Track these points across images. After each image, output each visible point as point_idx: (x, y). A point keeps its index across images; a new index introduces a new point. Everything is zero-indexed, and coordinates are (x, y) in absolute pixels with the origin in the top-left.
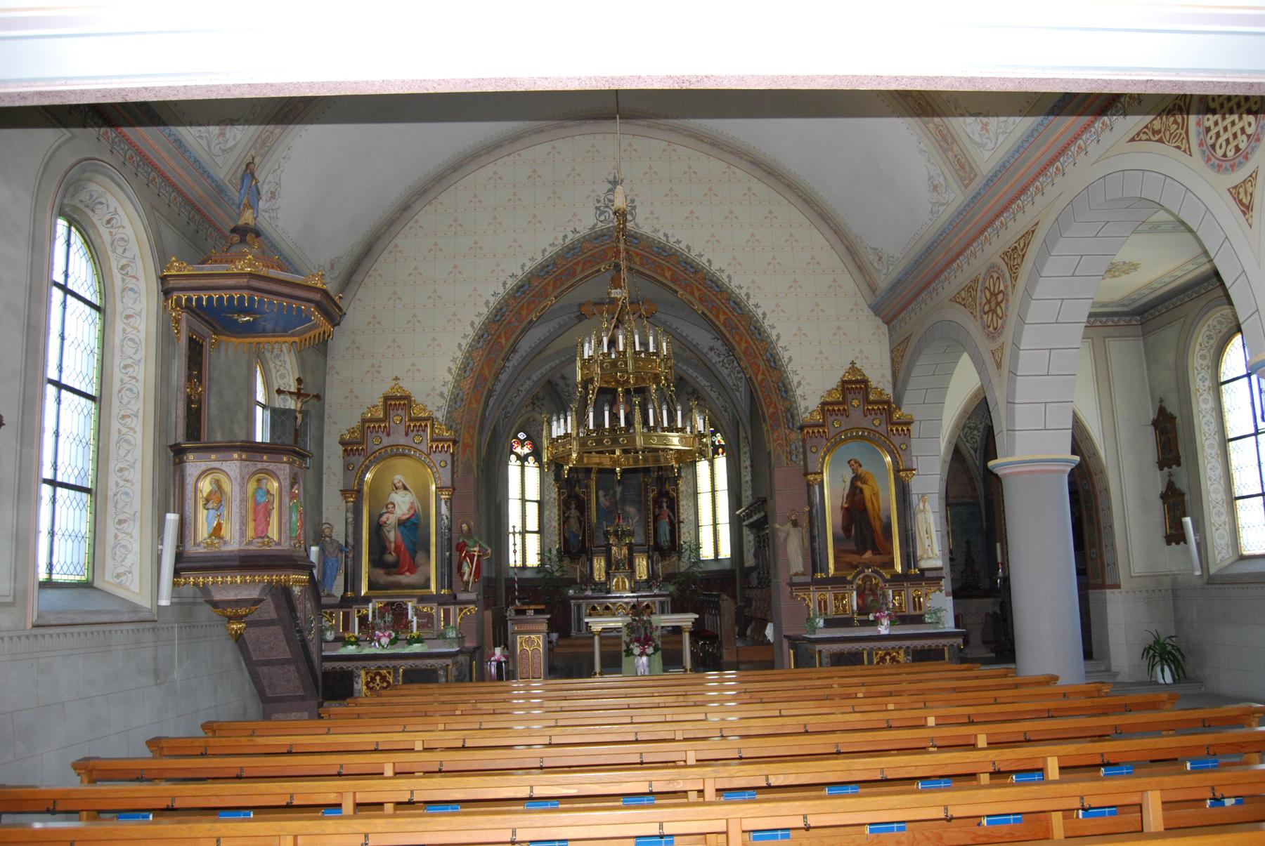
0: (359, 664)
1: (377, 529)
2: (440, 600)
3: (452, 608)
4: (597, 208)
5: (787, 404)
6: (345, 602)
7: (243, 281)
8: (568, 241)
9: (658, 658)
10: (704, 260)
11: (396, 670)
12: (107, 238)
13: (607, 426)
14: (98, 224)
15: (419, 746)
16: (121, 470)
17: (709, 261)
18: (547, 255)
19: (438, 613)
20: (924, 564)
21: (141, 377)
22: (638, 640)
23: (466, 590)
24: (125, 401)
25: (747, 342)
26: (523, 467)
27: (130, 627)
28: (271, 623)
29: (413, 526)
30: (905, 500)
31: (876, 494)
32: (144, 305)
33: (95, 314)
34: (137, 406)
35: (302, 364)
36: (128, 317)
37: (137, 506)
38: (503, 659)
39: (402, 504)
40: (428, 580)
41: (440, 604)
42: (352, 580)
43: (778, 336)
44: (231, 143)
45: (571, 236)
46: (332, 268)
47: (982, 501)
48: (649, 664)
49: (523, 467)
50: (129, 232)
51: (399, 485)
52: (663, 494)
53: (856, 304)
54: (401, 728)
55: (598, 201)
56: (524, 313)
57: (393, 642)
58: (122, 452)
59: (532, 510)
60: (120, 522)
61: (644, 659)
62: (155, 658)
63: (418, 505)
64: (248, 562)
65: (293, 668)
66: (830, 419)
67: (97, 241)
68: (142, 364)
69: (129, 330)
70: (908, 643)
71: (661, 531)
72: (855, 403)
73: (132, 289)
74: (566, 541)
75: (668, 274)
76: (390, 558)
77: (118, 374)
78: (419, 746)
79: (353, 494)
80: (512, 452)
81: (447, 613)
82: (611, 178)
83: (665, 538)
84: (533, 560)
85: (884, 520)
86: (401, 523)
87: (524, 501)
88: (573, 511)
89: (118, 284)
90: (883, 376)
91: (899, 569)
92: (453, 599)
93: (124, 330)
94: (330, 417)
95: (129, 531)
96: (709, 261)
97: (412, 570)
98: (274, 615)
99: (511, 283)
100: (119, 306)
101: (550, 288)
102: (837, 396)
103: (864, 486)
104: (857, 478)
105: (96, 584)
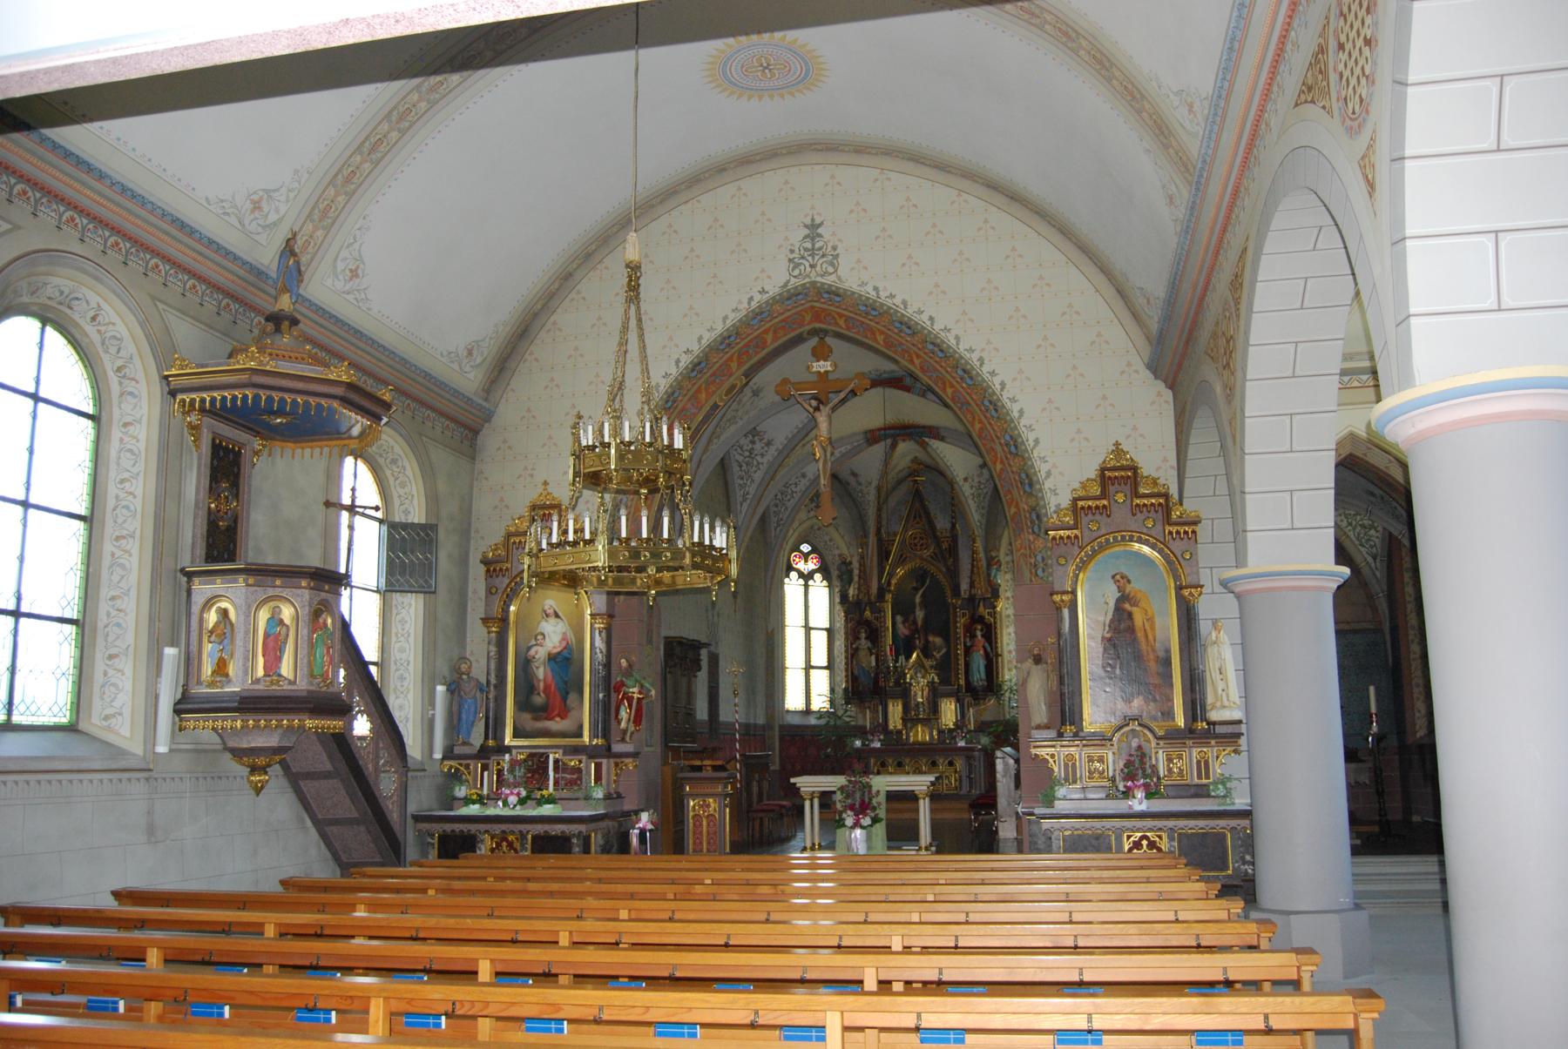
0: (482, 827)
1: (525, 664)
2: (591, 752)
3: (604, 761)
4: (790, 260)
5: (1032, 502)
6: (483, 753)
7: (244, 377)
8: (754, 304)
9: (880, 829)
10: (925, 317)
11: (523, 836)
12: (96, 338)
13: (666, 535)
14: (81, 322)
15: (897, 945)
16: (113, 598)
17: (931, 319)
18: (729, 323)
19: (588, 767)
20: (1214, 716)
21: (139, 492)
22: (852, 808)
23: (623, 740)
24: (120, 520)
25: (980, 422)
26: (806, 586)
27: (105, 776)
28: (325, 776)
29: (565, 661)
30: (1189, 629)
31: (1151, 620)
32: (145, 411)
33: (89, 423)
34: (134, 525)
35: (428, 473)
36: (126, 425)
37: (130, 638)
38: (650, 827)
39: (553, 635)
40: (581, 727)
41: (591, 757)
42: (494, 726)
43: (1021, 412)
44: (273, 217)
45: (757, 297)
46: (470, 352)
47: (1386, 626)
48: (869, 839)
49: (806, 586)
50: (121, 329)
51: (550, 611)
52: (977, 619)
53: (1129, 364)
54: (763, 917)
55: (792, 251)
56: (703, 396)
57: (522, 802)
58: (116, 578)
59: (820, 641)
60: (111, 657)
61: (858, 832)
62: (150, 813)
63: (571, 636)
64: (250, 704)
65: (362, 828)
66: (1085, 520)
67: (84, 342)
68: (141, 478)
69: (126, 439)
70: (1171, 823)
71: (974, 667)
72: (1120, 498)
73: (131, 393)
74: (853, 678)
75: (880, 338)
76: (539, 700)
77: (112, 489)
78: (897, 945)
79: (499, 623)
80: (790, 568)
81: (598, 767)
82: (808, 221)
83: (979, 676)
84: (820, 702)
85: (1161, 654)
86: (552, 658)
87: (808, 629)
88: (863, 641)
89: (115, 388)
90: (1165, 460)
91: (1180, 721)
92: (607, 751)
93: (121, 440)
94: (477, 531)
95: (121, 667)
96: (931, 319)
97: (563, 715)
98: (329, 767)
99: (685, 361)
100: (116, 413)
101: (734, 365)
102: (1096, 490)
103: (1135, 610)
104: (1124, 598)
105: (82, 726)
